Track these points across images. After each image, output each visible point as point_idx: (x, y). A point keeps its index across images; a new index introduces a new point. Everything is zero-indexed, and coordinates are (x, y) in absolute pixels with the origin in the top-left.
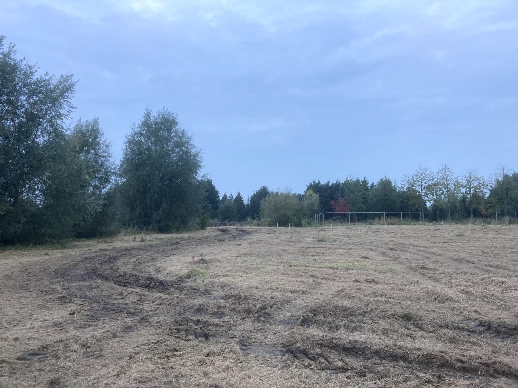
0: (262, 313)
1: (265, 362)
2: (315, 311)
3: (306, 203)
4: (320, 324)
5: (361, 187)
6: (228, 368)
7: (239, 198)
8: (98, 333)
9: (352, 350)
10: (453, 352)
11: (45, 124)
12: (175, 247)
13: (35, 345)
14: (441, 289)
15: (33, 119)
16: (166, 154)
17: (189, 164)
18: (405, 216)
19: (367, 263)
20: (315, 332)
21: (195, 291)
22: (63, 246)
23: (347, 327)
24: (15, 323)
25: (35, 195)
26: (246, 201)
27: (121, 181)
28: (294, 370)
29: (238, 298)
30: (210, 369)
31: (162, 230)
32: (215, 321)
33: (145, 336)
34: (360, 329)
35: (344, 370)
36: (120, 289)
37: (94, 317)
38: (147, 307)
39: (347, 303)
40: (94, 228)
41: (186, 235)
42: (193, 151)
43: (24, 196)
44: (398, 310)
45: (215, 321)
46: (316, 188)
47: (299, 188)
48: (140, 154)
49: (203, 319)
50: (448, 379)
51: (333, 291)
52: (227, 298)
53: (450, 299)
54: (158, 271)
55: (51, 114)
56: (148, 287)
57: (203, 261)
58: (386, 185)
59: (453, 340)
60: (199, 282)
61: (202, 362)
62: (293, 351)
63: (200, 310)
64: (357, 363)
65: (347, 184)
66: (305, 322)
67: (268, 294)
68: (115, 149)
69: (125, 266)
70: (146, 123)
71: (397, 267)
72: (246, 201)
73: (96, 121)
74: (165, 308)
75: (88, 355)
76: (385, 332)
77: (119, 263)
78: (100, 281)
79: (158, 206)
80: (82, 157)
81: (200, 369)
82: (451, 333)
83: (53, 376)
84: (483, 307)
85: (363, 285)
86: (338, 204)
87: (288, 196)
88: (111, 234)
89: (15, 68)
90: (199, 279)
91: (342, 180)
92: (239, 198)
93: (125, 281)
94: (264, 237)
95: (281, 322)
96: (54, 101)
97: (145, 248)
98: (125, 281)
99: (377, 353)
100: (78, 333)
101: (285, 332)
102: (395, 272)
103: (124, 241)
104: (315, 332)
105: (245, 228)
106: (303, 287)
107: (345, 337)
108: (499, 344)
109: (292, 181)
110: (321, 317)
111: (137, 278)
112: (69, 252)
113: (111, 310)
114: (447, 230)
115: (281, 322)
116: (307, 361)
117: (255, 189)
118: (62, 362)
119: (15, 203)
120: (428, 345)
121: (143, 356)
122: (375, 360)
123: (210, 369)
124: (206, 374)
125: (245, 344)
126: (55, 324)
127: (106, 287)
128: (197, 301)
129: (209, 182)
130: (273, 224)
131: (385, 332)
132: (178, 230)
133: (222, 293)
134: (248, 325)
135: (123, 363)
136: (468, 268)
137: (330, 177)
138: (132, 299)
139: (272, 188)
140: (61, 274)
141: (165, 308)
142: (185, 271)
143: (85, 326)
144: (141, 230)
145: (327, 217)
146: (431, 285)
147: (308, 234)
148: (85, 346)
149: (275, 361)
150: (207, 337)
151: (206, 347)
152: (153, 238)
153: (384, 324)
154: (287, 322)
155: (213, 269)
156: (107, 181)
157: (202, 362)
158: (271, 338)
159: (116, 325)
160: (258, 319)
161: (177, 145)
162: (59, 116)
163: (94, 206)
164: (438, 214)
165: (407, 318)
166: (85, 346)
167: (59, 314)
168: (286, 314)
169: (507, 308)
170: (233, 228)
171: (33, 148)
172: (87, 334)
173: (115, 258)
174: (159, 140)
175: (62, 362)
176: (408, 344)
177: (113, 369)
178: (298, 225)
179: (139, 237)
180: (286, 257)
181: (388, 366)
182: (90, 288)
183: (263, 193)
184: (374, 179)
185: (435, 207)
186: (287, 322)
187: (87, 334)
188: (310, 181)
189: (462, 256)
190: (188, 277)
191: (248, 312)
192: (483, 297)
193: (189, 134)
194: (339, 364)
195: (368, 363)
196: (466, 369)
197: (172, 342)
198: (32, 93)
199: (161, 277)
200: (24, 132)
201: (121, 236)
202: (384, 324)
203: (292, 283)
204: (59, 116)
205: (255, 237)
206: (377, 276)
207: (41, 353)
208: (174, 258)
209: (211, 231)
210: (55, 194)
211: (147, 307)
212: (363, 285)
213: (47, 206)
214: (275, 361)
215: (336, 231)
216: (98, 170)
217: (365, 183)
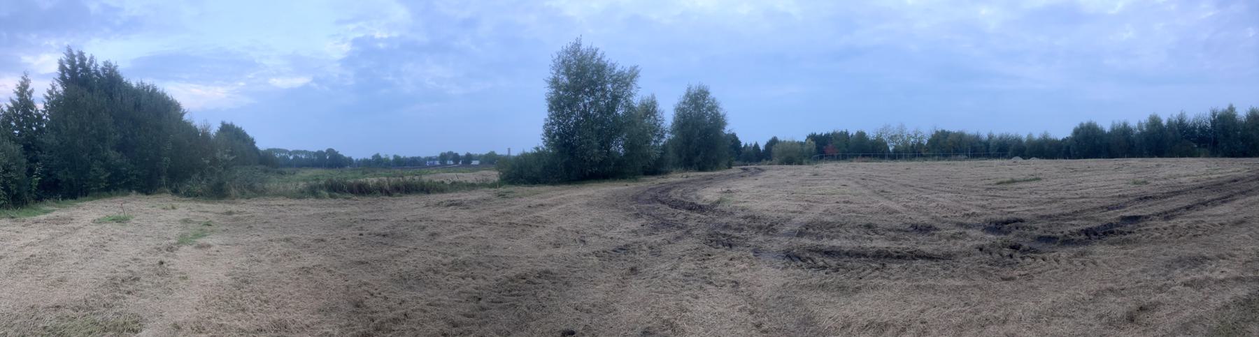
0: (770, 228)
1: (771, 265)
2: (807, 226)
3: (806, 148)
4: (811, 235)
5: (844, 136)
6: (744, 270)
7: (756, 146)
8: (659, 240)
9: (829, 253)
10: (893, 246)
11: (623, 101)
12: (710, 181)
13: (622, 243)
14: (893, 205)
15: (615, 98)
16: (702, 116)
17: (718, 122)
18: (875, 156)
19: (846, 190)
20: (807, 241)
21: (723, 213)
22: (637, 180)
23: (828, 236)
24: (611, 227)
25: (619, 148)
26: (762, 147)
27: (672, 136)
28: (791, 270)
29: (754, 218)
30: (732, 269)
31: (701, 170)
32: (737, 234)
33: (689, 244)
34: (837, 237)
35: (824, 268)
36: (672, 210)
37: (656, 229)
38: (691, 223)
39: (829, 219)
40: (655, 168)
41: (718, 173)
42: (721, 113)
43: (612, 149)
44: (864, 222)
45: (737, 234)
46: (813, 137)
47: (802, 138)
48: (684, 117)
49: (728, 233)
50: (888, 265)
51: (821, 211)
52: (745, 218)
53: (897, 212)
54: (698, 198)
55: (626, 93)
56: (690, 209)
57: (729, 191)
58: (861, 135)
59: (894, 239)
60: (726, 207)
61: (727, 265)
62: (790, 256)
63: (726, 226)
64: (833, 262)
65: (834, 134)
66: (800, 234)
67: (774, 215)
68: (667, 115)
69: (675, 195)
70: (688, 95)
71: (866, 192)
72: (762, 147)
73: (653, 97)
74: (703, 224)
75: (653, 254)
76: (854, 238)
77: (672, 193)
78: (659, 205)
79: (697, 153)
80: (646, 121)
81: (726, 269)
82: (893, 234)
83: (633, 265)
84: (914, 215)
85: (842, 205)
86: (828, 148)
87: (793, 143)
88: (666, 173)
89: (604, 67)
90: (726, 205)
91: (831, 132)
92: (756, 146)
93: (676, 205)
94: (775, 173)
95: (784, 235)
96: (627, 85)
97: (689, 182)
98: (676, 205)
99: (847, 254)
100: (646, 239)
101: (785, 242)
102: (864, 195)
103: (675, 177)
104: (807, 241)
105: (762, 167)
106: (800, 209)
107: (826, 243)
108: (920, 238)
109: (796, 132)
110: (811, 230)
111: (683, 204)
112: (641, 184)
113: (668, 225)
114: (901, 165)
115: (784, 235)
116: (800, 263)
117: (770, 138)
118: (637, 257)
119: (609, 152)
120: (880, 244)
121: (687, 258)
122: (847, 258)
123: (732, 269)
124: (730, 273)
125: (757, 252)
126: (633, 231)
127: (664, 209)
128: (725, 220)
129: (734, 135)
130: (782, 163)
131: (854, 238)
132: (712, 170)
133: (742, 214)
134: (760, 238)
135: (675, 261)
136: (910, 190)
137: (823, 129)
138: (681, 217)
139: (781, 138)
140: (636, 198)
141: (703, 224)
142: (717, 198)
143: (651, 234)
144: (686, 170)
145: (821, 158)
146: (885, 203)
147: (806, 170)
148: (651, 248)
149: (778, 264)
150: (730, 246)
151: (730, 254)
152: (693, 175)
153: (854, 232)
154: (788, 235)
155: (736, 197)
156: (663, 137)
157: (727, 265)
158: (776, 247)
159: (669, 236)
160: (767, 233)
161: (709, 109)
162: (630, 95)
163: (656, 155)
164: (897, 155)
165: (869, 226)
166: (651, 248)
167: (635, 225)
168: (788, 228)
169: (927, 214)
170: (752, 167)
171: (616, 118)
172: (652, 239)
173: (669, 189)
174: (697, 107)
175: (637, 257)
176: (868, 245)
177: (668, 265)
178: (801, 164)
179: (685, 174)
180: (790, 188)
181: (855, 262)
182: (654, 209)
183: (774, 142)
184: (853, 131)
185: (895, 151)
186: (788, 235)
187: (652, 239)
188: (809, 133)
189: (908, 182)
190: (718, 202)
191: (760, 228)
192: (916, 208)
193: (718, 100)
194: (821, 264)
195: (841, 262)
196: (900, 257)
197: (706, 249)
198: (615, 81)
199: (700, 203)
200: (611, 108)
201: (673, 174)
202: (854, 232)
203: (793, 207)
204: (630, 95)
205: (768, 173)
206: (851, 198)
207: (625, 249)
208: (709, 189)
209: (736, 170)
210: (631, 146)
211: (691, 223)
212: (842, 205)
213: (626, 155)
214: (778, 264)
215: (827, 167)
216: (656, 130)
217: (847, 133)
